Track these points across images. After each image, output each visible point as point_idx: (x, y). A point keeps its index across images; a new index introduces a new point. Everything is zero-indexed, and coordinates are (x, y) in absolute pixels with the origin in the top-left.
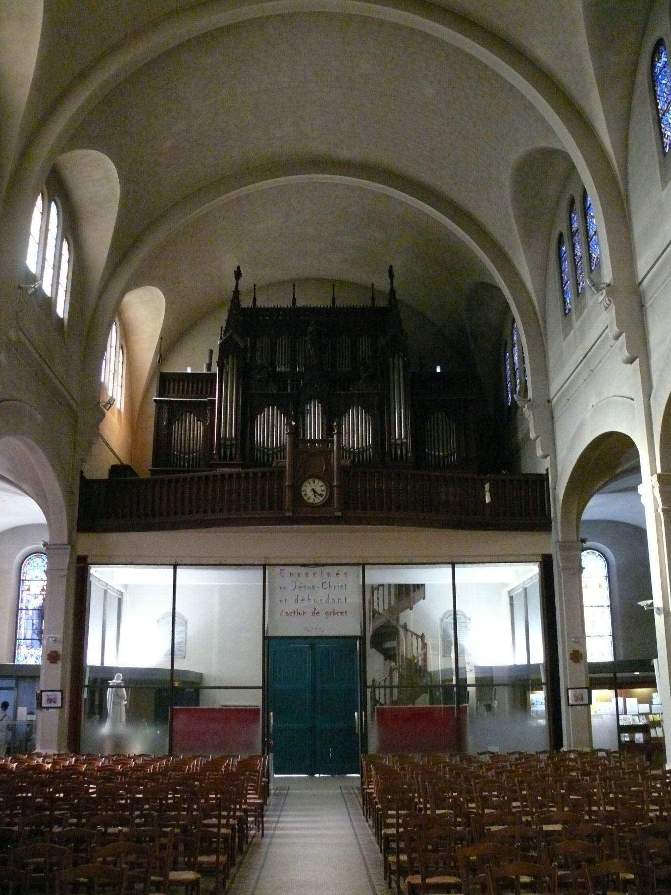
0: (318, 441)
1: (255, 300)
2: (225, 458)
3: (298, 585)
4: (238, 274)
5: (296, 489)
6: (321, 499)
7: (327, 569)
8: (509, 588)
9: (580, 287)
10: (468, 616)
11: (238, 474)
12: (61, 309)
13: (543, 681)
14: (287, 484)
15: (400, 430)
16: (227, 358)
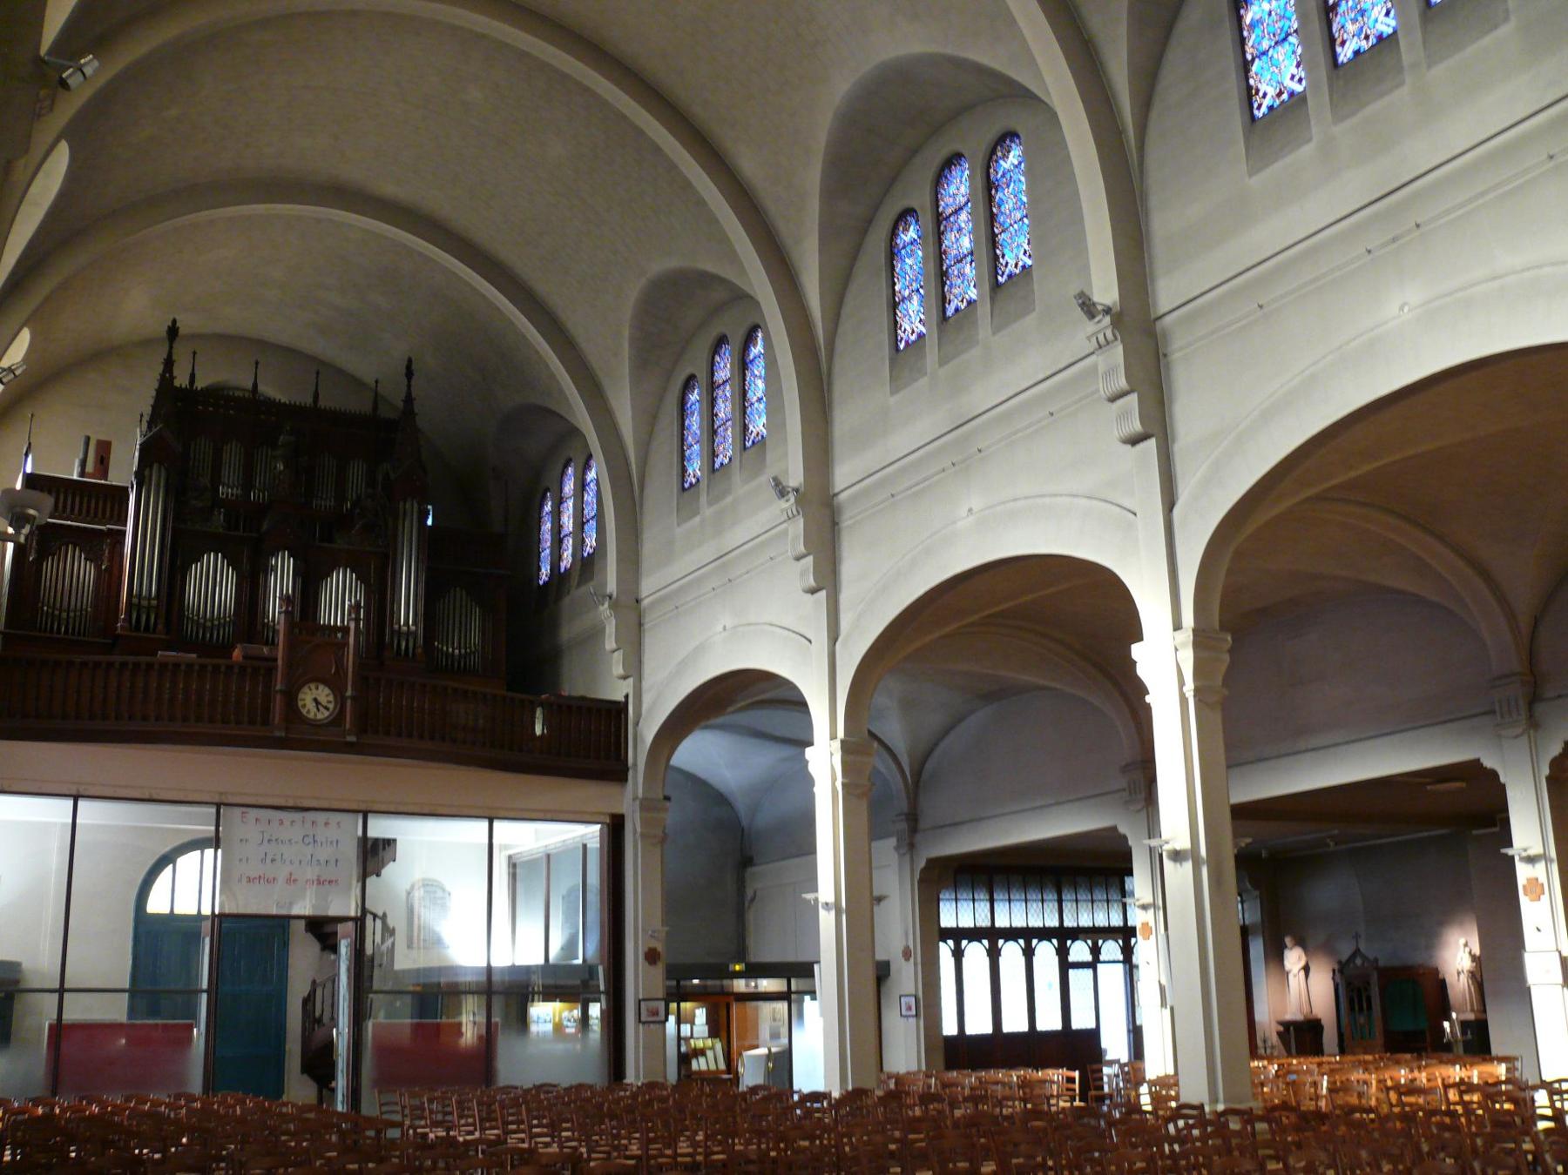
2: (137, 628)
3: (267, 837)
5: (291, 697)
6: (327, 714)
7: (310, 816)
8: (511, 852)
10: (448, 888)
11: (190, 666)
13: (602, 988)
14: (278, 687)
15: (406, 612)
16: (151, 467)
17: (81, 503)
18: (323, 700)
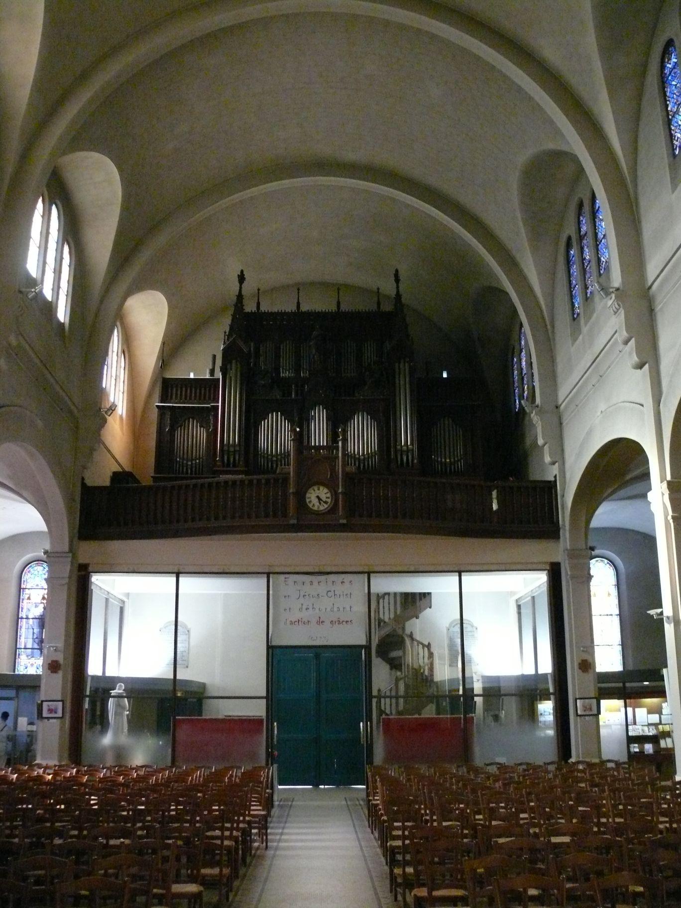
0: (323, 447)
1: (258, 304)
2: (228, 465)
3: (302, 593)
4: (242, 278)
5: (301, 496)
6: (326, 506)
7: (332, 577)
8: (517, 597)
9: (589, 291)
10: (475, 625)
11: (242, 481)
12: (62, 314)
13: (551, 690)
14: (291, 491)
15: (406, 436)
16: (231, 363)
17: (191, 392)
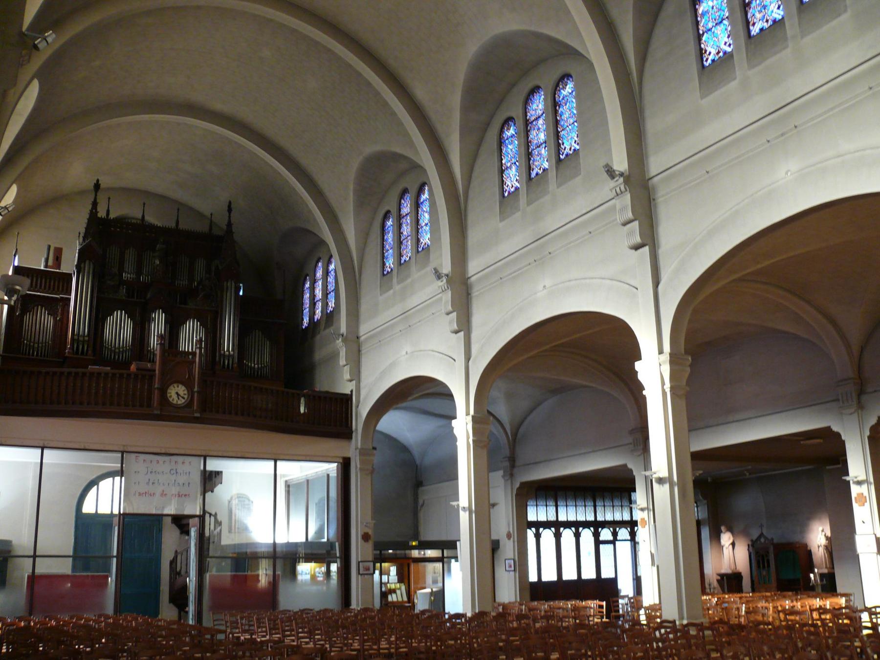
2: (77, 352)
3: (150, 470)
5: (163, 392)
6: (183, 401)
7: (174, 458)
8: (287, 479)
10: (251, 499)
11: (107, 374)
13: (338, 555)
14: (156, 386)
15: (228, 344)
16: (85, 262)
17: (45, 283)
18: (181, 393)
